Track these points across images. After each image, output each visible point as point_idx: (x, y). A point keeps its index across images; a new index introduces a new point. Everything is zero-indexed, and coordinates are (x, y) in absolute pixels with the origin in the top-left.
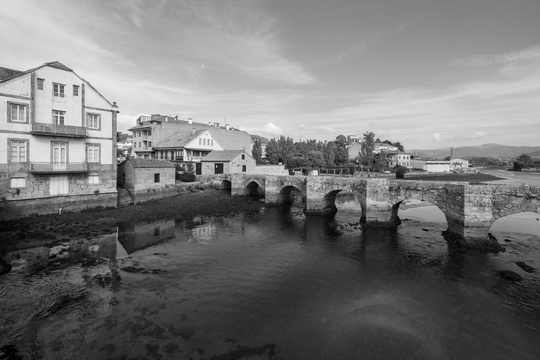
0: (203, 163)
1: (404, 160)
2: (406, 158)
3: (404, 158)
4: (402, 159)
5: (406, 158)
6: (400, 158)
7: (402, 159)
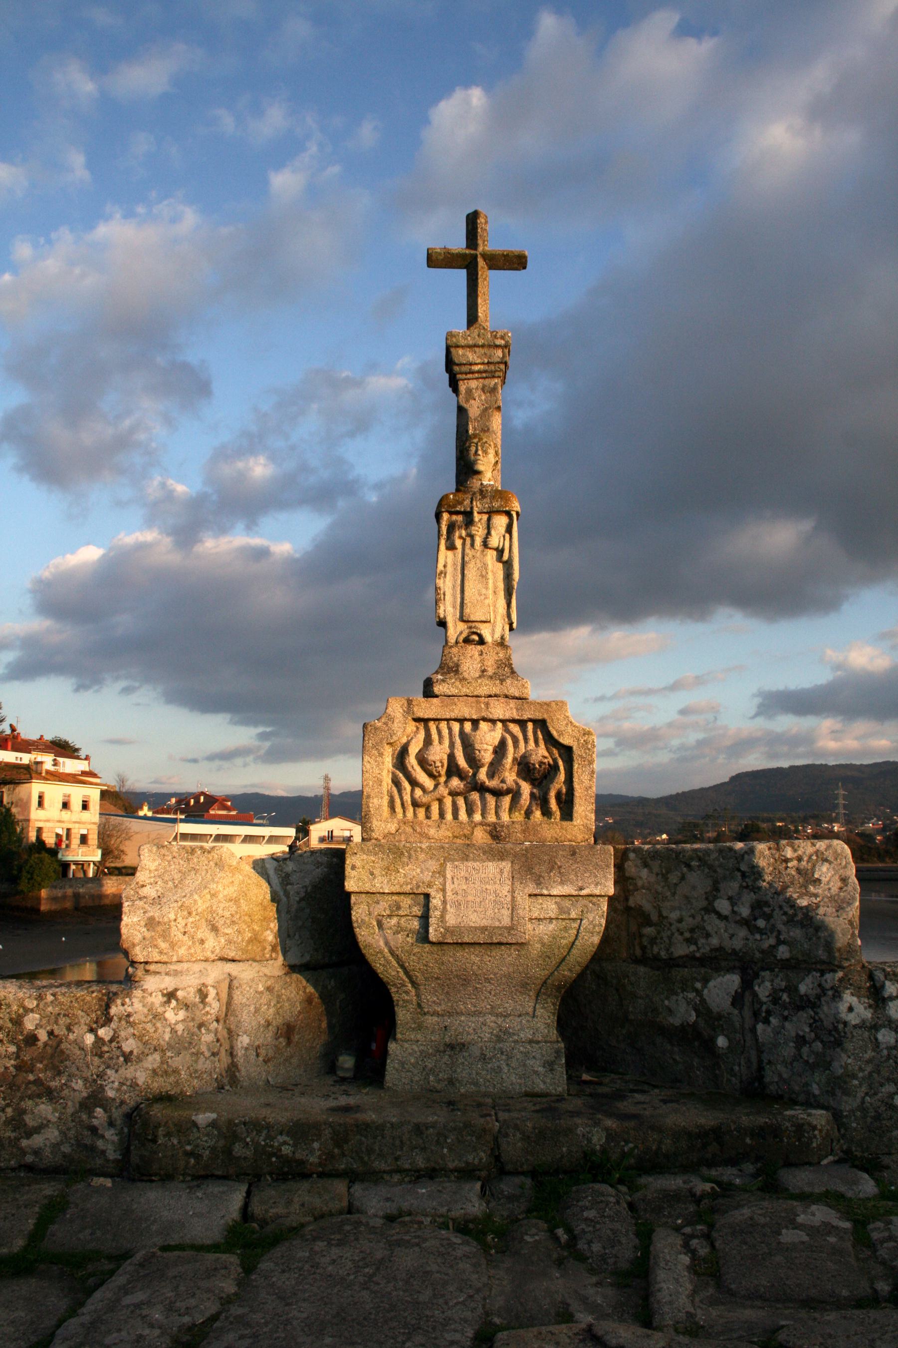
0: (481, 722)
1: (66, 815)
2: (76, 804)
3: (65, 805)
4: (53, 809)
5: (76, 804)
6: (41, 804)
7: (53, 809)
